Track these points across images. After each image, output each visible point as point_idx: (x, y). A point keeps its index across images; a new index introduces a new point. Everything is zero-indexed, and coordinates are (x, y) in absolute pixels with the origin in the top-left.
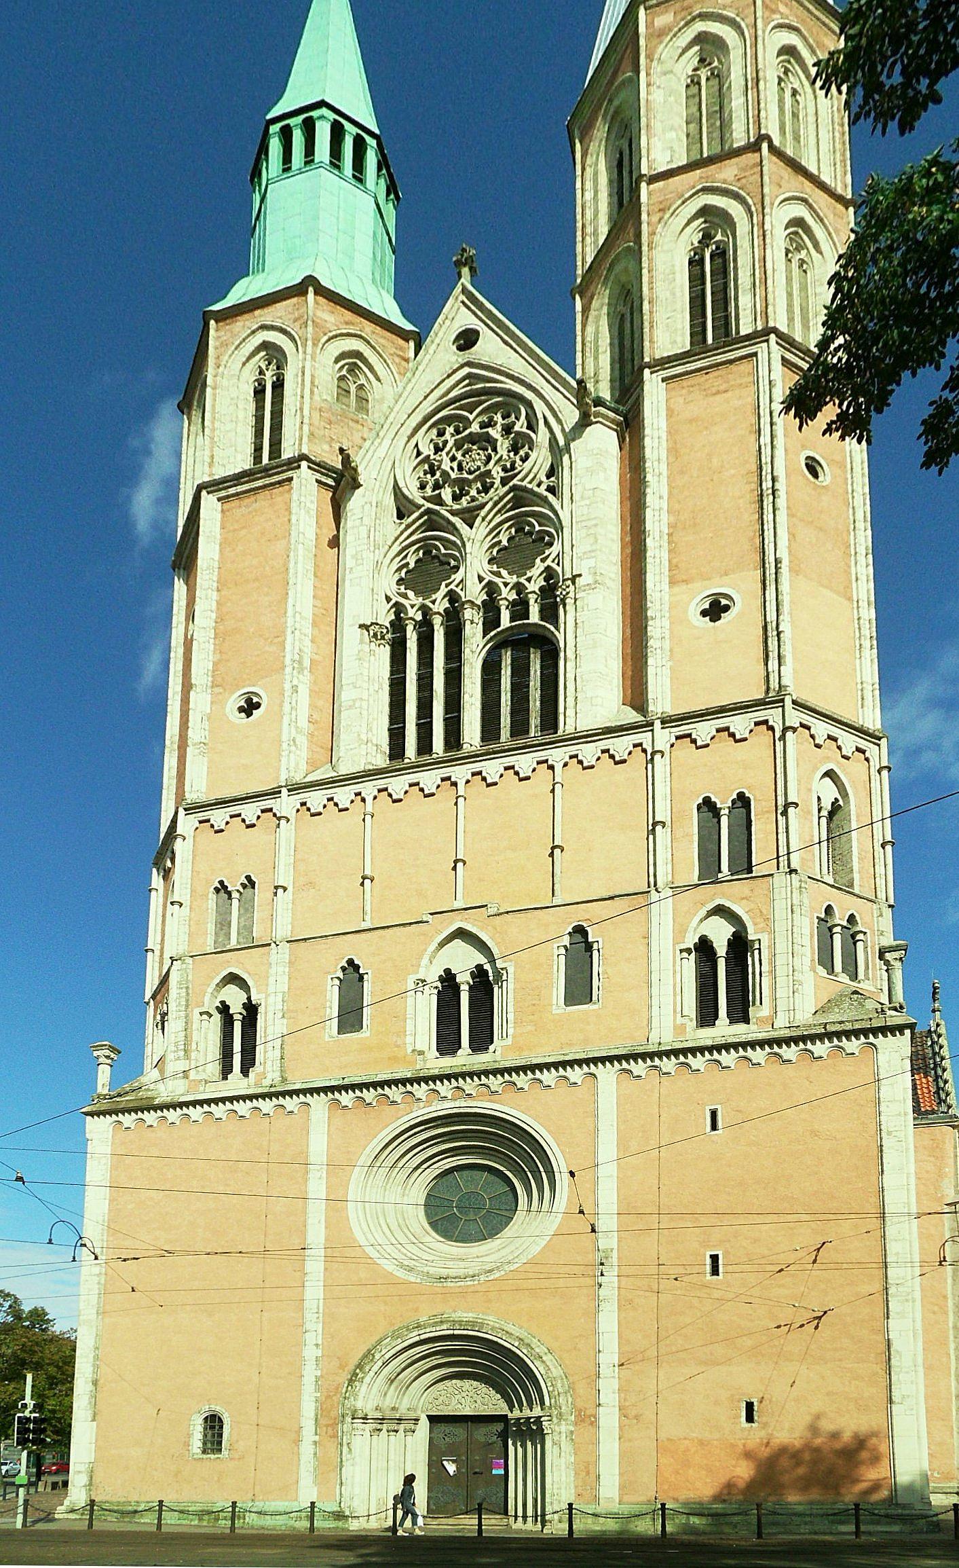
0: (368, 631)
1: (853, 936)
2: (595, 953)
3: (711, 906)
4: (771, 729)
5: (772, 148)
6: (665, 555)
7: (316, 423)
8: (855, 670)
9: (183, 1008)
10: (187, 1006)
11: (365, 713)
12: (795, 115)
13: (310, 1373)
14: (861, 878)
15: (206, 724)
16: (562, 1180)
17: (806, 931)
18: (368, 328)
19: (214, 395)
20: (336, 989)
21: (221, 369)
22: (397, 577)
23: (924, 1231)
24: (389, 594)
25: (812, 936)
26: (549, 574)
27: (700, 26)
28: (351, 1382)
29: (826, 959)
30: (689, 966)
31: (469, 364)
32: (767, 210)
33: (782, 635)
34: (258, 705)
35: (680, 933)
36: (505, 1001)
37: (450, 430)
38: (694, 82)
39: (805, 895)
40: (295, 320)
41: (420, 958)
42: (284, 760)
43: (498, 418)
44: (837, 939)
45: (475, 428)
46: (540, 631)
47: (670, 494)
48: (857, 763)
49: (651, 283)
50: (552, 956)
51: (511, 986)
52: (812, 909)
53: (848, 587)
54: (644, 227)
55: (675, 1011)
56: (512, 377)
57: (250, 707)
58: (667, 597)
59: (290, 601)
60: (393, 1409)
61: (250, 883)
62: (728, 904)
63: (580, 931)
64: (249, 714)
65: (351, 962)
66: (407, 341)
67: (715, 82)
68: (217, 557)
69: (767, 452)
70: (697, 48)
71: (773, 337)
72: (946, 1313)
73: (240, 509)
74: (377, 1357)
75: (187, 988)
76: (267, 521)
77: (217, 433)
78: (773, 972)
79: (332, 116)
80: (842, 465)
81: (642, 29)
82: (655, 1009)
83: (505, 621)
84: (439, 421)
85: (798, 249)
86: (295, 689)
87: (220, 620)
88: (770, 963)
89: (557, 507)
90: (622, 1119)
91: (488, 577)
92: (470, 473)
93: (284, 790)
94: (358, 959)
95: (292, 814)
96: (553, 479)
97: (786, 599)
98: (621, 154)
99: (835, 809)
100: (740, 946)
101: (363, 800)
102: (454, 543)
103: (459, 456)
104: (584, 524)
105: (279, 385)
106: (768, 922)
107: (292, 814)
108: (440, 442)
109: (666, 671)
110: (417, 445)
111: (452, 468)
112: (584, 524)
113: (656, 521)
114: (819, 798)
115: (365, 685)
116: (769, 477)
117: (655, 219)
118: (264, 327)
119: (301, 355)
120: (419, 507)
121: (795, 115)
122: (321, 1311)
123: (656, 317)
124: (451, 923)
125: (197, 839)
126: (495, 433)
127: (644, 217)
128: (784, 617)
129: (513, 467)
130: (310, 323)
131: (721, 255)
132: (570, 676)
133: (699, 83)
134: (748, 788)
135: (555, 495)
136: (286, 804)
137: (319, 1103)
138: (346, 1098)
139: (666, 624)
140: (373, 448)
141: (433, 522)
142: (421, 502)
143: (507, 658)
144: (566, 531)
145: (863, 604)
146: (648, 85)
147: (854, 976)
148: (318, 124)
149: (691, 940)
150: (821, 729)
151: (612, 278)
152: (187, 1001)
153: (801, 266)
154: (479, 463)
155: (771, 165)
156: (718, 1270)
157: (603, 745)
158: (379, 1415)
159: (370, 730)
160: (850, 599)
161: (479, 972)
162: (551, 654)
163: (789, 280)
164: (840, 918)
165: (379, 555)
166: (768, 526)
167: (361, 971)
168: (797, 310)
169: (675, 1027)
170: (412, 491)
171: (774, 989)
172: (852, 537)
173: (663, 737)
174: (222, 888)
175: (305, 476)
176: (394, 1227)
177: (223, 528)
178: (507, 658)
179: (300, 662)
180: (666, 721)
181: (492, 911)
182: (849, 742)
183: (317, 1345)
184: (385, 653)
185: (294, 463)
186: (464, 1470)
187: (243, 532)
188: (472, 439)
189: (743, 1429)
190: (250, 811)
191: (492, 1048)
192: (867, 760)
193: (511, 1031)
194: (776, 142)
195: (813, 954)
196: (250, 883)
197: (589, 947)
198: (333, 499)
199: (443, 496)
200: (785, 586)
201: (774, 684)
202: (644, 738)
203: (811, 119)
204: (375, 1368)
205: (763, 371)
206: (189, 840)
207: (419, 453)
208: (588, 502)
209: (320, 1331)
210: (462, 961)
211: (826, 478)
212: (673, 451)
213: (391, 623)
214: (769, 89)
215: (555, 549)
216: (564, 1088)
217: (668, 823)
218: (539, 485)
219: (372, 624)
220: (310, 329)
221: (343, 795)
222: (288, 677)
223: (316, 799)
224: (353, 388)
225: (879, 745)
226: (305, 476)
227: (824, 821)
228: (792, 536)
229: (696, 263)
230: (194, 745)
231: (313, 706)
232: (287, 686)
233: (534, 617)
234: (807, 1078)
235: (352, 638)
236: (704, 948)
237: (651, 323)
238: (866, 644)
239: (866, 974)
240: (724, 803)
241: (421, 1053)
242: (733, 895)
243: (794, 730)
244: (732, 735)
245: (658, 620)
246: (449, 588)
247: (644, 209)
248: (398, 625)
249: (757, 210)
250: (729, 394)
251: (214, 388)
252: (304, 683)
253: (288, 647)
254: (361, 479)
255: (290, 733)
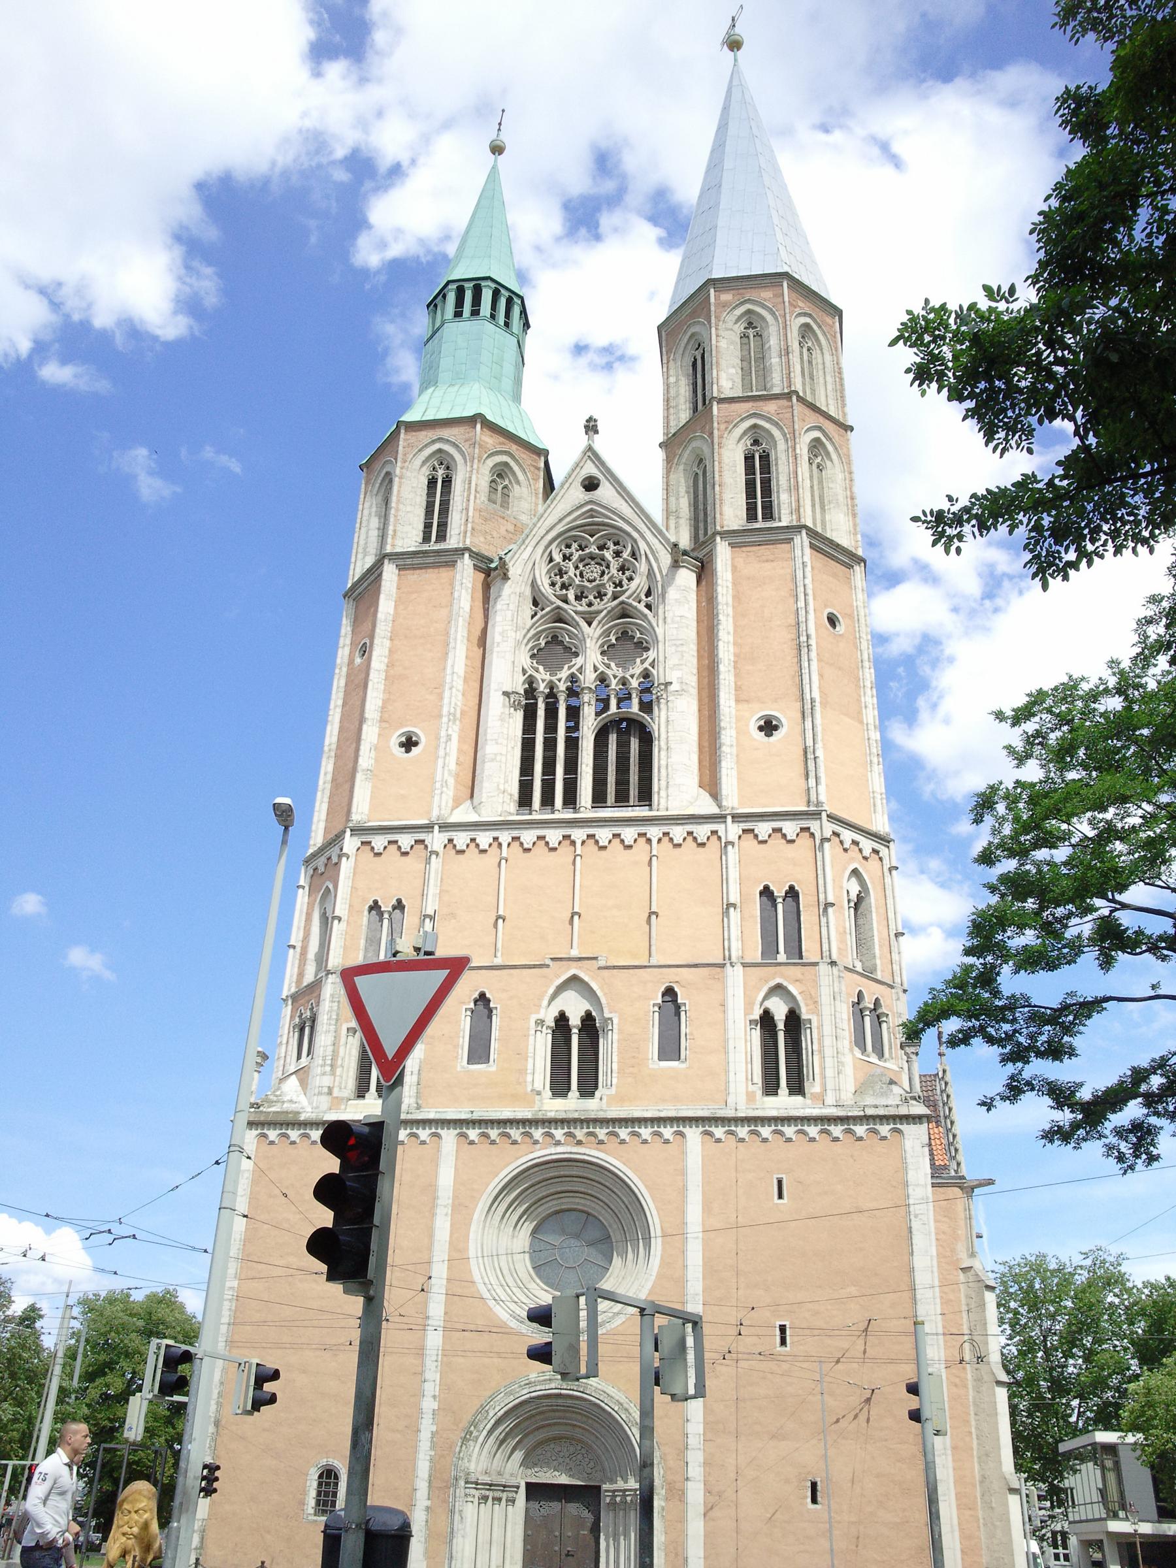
0: (509, 697)
1: (878, 1017)
2: (683, 1014)
3: (772, 983)
4: (812, 835)
5: (798, 397)
6: (732, 678)
7: (476, 521)
8: (868, 781)
9: (333, 1022)
10: (337, 1020)
11: (503, 766)
12: (810, 362)
13: (427, 1427)
14: (882, 964)
15: (373, 754)
16: (657, 1245)
17: (845, 1016)
18: (514, 448)
19: (400, 483)
20: (469, 1019)
21: (407, 464)
22: (530, 653)
23: (944, 1295)
24: (526, 667)
25: (849, 1020)
26: (646, 675)
27: (748, 306)
28: (465, 1440)
29: (860, 1042)
30: (757, 1034)
31: (591, 502)
32: (797, 440)
33: (817, 760)
34: (416, 744)
35: (749, 1006)
36: (610, 1049)
37: (575, 546)
38: (744, 336)
39: (843, 983)
40: (466, 441)
41: (541, 999)
42: (437, 798)
43: (610, 544)
44: (867, 1020)
45: (593, 549)
46: (640, 719)
47: (735, 631)
48: (874, 862)
49: (720, 472)
50: (649, 1012)
51: (615, 1037)
52: (849, 994)
53: (860, 713)
54: (716, 432)
55: (747, 1079)
56: (623, 519)
57: (409, 744)
58: (734, 711)
59: (450, 662)
60: (500, 1474)
61: (399, 906)
62: (785, 984)
63: (670, 992)
64: (408, 751)
65: (482, 996)
66: (539, 457)
67: (758, 338)
68: (392, 613)
69: (802, 613)
70: (747, 317)
71: (804, 532)
72: (966, 1386)
73: (413, 577)
74: (491, 1414)
75: (339, 1002)
76: (433, 590)
77: (400, 513)
78: (821, 1051)
79: (493, 285)
80: (851, 616)
81: (712, 300)
82: (732, 1074)
83: (613, 708)
84: (567, 539)
85: (816, 456)
86: (449, 738)
87: (390, 665)
88: (819, 1044)
89: (655, 625)
90: (706, 1182)
91: (602, 668)
92: (590, 581)
93: (436, 827)
94: (490, 993)
95: (440, 849)
96: (649, 599)
97: (819, 729)
98: (695, 360)
99: (860, 900)
100: (794, 1021)
101: (500, 845)
102: (576, 635)
103: (581, 565)
104: (674, 642)
105: (447, 482)
106: (817, 1010)
107: (440, 849)
108: (568, 551)
109: (734, 773)
110: (551, 552)
111: (575, 575)
112: (674, 642)
113: (726, 652)
114: (848, 892)
115: (505, 742)
116: (805, 633)
117: (723, 427)
118: (440, 440)
119: (468, 469)
120: (552, 603)
121: (810, 362)
122: (440, 1359)
123: (725, 496)
124: (569, 969)
125: (358, 858)
126: (608, 555)
127: (715, 425)
128: (819, 745)
129: (620, 584)
130: (477, 446)
131: (765, 458)
132: (663, 763)
133: (748, 337)
134: (796, 882)
135: (651, 611)
136: (437, 840)
137: (449, 1136)
138: (473, 1134)
139: (734, 733)
140: (520, 552)
141: (559, 617)
142: (553, 599)
143: (613, 738)
144: (661, 645)
145: (871, 727)
146: (717, 336)
147: (881, 1055)
148: (484, 290)
149: (757, 1014)
150: (848, 836)
151: (690, 448)
152: (338, 1015)
153: (818, 467)
154: (595, 575)
155: (798, 408)
156: (780, 1330)
157: (689, 828)
158: (487, 1479)
159: (506, 782)
160: (861, 722)
161: (588, 1019)
162: (647, 740)
163: (811, 477)
164: (868, 1003)
165: (520, 635)
166: (805, 671)
167: (492, 1005)
168: (817, 499)
169: (747, 1092)
170: (547, 590)
171: (823, 1069)
172: (861, 673)
173: (732, 830)
174: (375, 907)
175: (466, 564)
176: (506, 1272)
177: (398, 588)
178: (613, 738)
179: (454, 715)
180: (737, 818)
181: (602, 963)
182: (867, 845)
183: (434, 1397)
184: (519, 716)
185: (459, 552)
186: (557, 1548)
187: (414, 596)
188: (592, 557)
189: (463, 1067)
190: (406, 841)
191: (598, 1094)
192: (881, 859)
193: (615, 1081)
194: (801, 394)
195: (851, 1036)
196: (399, 906)
197: (678, 1008)
198: (485, 580)
199: (569, 596)
200: (818, 715)
201: (813, 798)
202: (720, 828)
203: (821, 367)
204: (489, 1426)
205: (798, 552)
206: (352, 859)
207: (551, 560)
208: (676, 626)
209: (438, 1382)
210: (575, 1008)
211: (840, 629)
212: (737, 597)
213: (526, 691)
214: (795, 359)
215: (651, 655)
216: (657, 1144)
217: (738, 905)
218: (639, 602)
219: (513, 692)
220: (477, 451)
221: (484, 839)
222: (444, 726)
223: (461, 839)
224: (500, 488)
225: (888, 847)
226: (466, 564)
227: (852, 910)
228: (821, 676)
229: (749, 459)
230: (363, 770)
231: (460, 751)
232: (443, 733)
233: (635, 708)
234: (852, 1156)
235: (495, 705)
236: (766, 1020)
237: (721, 500)
238: (875, 760)
239: (890, 1053)
240: (779, 892)
241: (539, 1093)
242: (789, 977)
243: (829, 840)
244: (784, 836)
245: (728, 731)
246: (572, 671)
247: (715, 419)
248: (530, 692)
249: (792, 438)
250: (774, 564)
251: (401, 478)
252: (455, 731)
253: (446, 701)
254: (510, 574)
255: (443, 774)
